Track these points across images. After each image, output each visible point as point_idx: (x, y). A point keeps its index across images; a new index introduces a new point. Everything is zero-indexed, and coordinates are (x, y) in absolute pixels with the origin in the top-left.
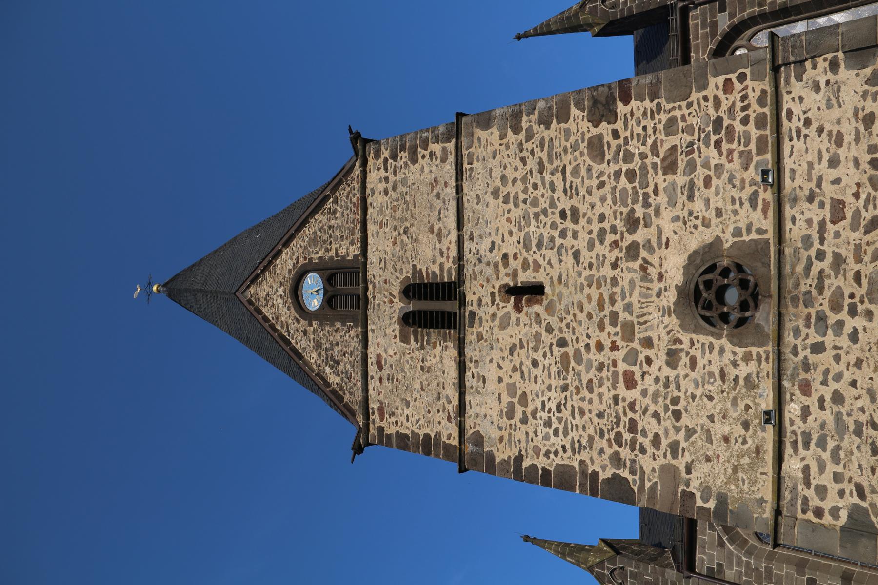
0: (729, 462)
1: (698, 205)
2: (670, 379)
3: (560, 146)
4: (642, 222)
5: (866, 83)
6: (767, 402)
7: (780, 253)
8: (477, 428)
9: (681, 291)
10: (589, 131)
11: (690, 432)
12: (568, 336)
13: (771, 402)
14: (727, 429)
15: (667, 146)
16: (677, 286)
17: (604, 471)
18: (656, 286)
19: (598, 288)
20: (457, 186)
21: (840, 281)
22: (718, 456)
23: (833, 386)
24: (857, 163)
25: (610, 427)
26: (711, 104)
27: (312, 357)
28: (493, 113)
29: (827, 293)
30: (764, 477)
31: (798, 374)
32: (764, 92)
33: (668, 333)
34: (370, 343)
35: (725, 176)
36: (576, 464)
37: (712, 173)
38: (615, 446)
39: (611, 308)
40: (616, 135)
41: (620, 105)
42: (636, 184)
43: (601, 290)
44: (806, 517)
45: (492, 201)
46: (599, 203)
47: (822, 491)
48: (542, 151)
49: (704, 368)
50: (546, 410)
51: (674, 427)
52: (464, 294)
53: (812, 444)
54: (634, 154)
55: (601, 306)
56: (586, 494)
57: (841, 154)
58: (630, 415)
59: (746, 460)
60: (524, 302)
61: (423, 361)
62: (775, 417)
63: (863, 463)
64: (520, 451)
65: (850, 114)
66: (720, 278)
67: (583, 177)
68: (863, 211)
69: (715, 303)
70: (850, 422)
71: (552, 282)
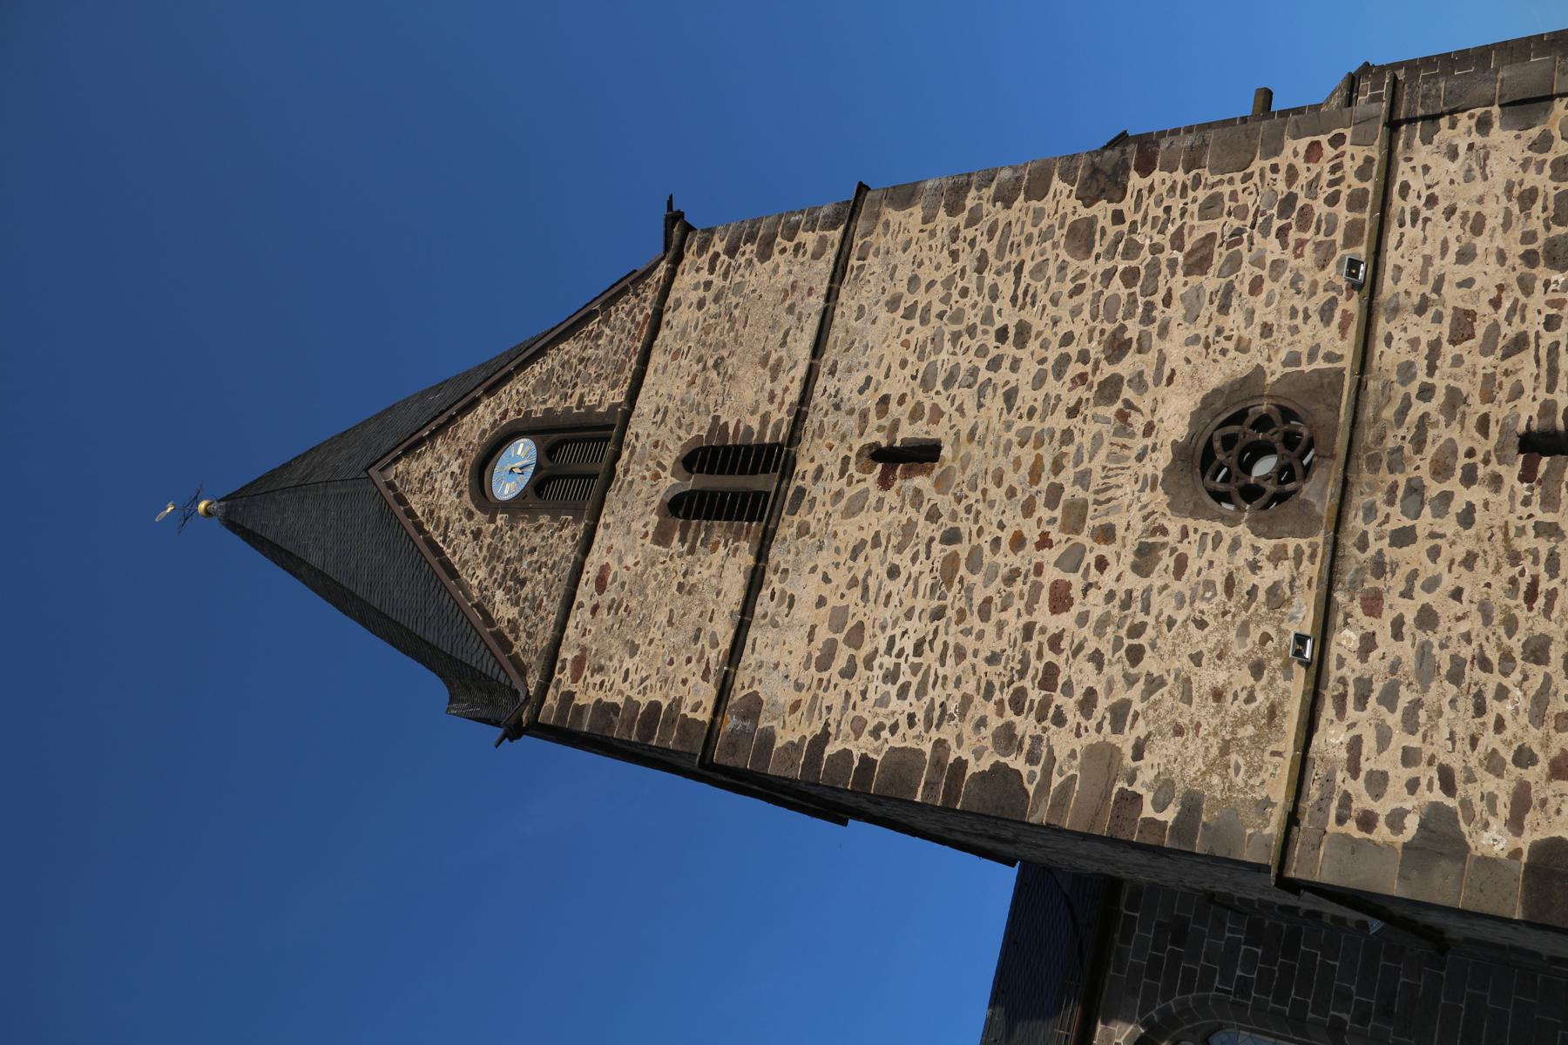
0: (1215, 734)
2: (1135, 594)
4: (1135, 345)
7: (1360, 387)
8: (756, 687)
11: (1154, 684)
12: (965, 526)
14: (1221, 677)
15: (1199, 235)
17: (978, 759)
19: (1035, 448)
21: (1454, 432)
22: (1198, 725)
23: (1421, 598)
24: (1502, 257)
25: (1006, 680)
26: (1281, 176)
29: (1430, 451)
31: (1363, 581)
32: (1369, 161)
36: (927, 748)
37: (1265, 273)
39: (1052, 479)
42: (1137, 289)
44: (1342, 830)
47: (1378, 783)
49: (1199, 573)
50: (895, 651)
53: (1372, 700)
54: (1141, 247)
58: (1049, 656)
59: (1249, 730)
63: (1457, 729)
64: (827, 724)
65: (1500, 190)
70: (1444, 659)
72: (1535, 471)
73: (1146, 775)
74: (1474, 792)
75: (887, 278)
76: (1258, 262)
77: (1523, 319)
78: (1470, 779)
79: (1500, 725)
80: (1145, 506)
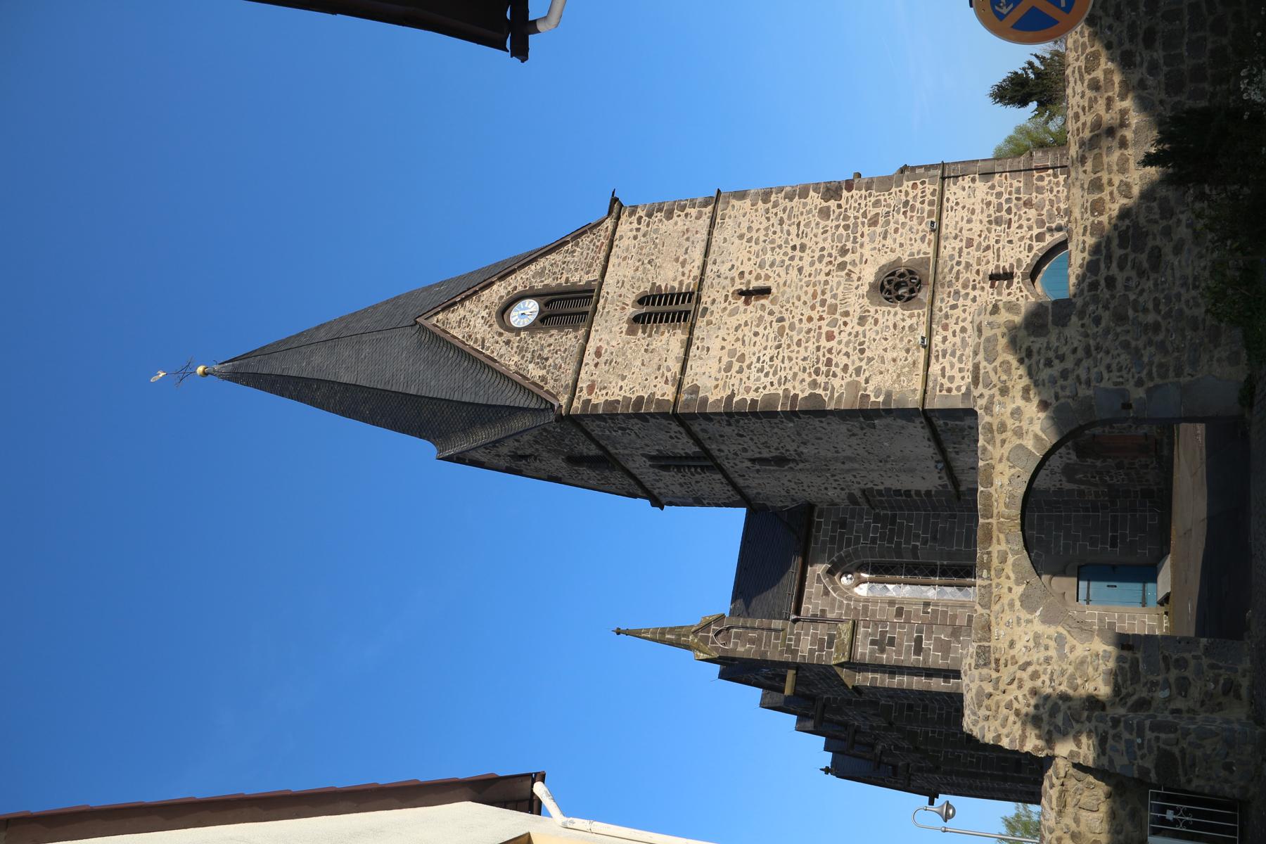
1: (889, 242)
11: (870, 360)
14: (895, 355)
21: (968, 275)
24: (981, 222)
29: (961, 281)
40: (839, 206)
47: (952, 379)
58: (828, 355)
76: (897, 222)
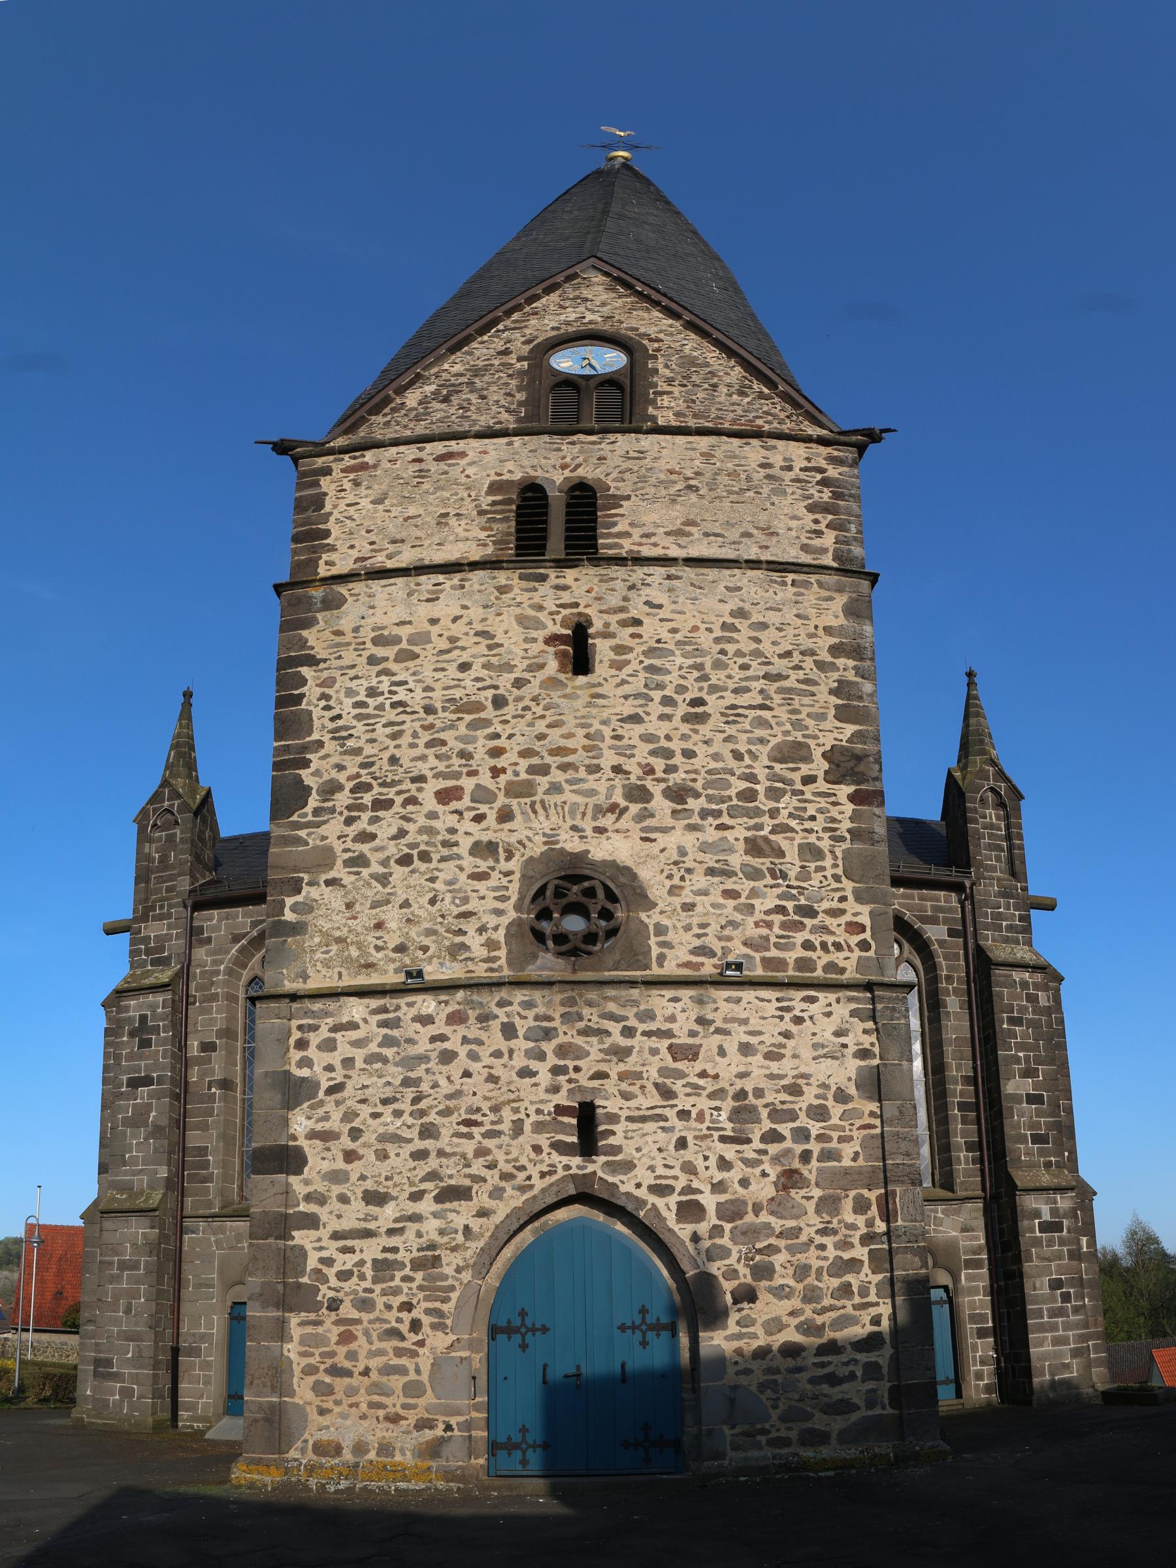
0: (350, 931)
1: (700, 880)
2: (455, 848)
3: (802, 705)
4: (680, 807)
5: (839, 1088)
6: (434, 972)
7: (632, 983)
8: (350, 599)
9: (581, 858)
10: (819, 745)
11: (383, 879)
12: (510, 710)
13: (434, 977)
14: (393, 925)
15: (785, 845)
16: (588, 852)
17: (312, 774)
18: (588, 825)
19: (584, 747)
20: (760, 562)
21: (595, 1055)
22: (355, 918)
23: (463, 1051)
24: (743, 1075)
25: (377, 774)
26: (835, 904)
27: (455, 366)
28: (868, 622)
29: (580, 1041)
30: (337, 977)
31: (473, 1008)
32: (843, 970)
33: (520, 842)
34: (487, 441)
35: (738, 917)
36: (315, 736)
37: (743, 900)
38: (351, 784)
39: (554, 766)
40: (808, 780)
41: (851, 789)
42: (735, 802)
43: (580, 751)
44: (294, 1030)
45: (727, 608)
46: (711, 751)
47: (329, 1046)
48: (798, 681)
49: (473, 891)
50: (394, 688)
51: (388, 858)
52: (576, 566)
53: (386, 1031)
54: (778, 801)
55: (557, 752)
56: (274, 756)
57: (755, 1058)
58: (399, 800)
59: (354, 952)
60: (562, 647)
61: (458, 515)
62: (415, 983)
63: (370, 1089)
64: (325, 661)
65: (803, 1069)
66: (599, 907)
67: (751, 732)
68: (684, 1082)
69: (564, 901)
70: (419, 1072)
71: (594, 686)
72: (563, 1115)
73: (314, 892)
74: (330, 1107)
75: (768, 605)
76: (754, 893)
77: (688, 1095)
78: (338, 1103)
79: (375, 1116)
80: (530, 839)
